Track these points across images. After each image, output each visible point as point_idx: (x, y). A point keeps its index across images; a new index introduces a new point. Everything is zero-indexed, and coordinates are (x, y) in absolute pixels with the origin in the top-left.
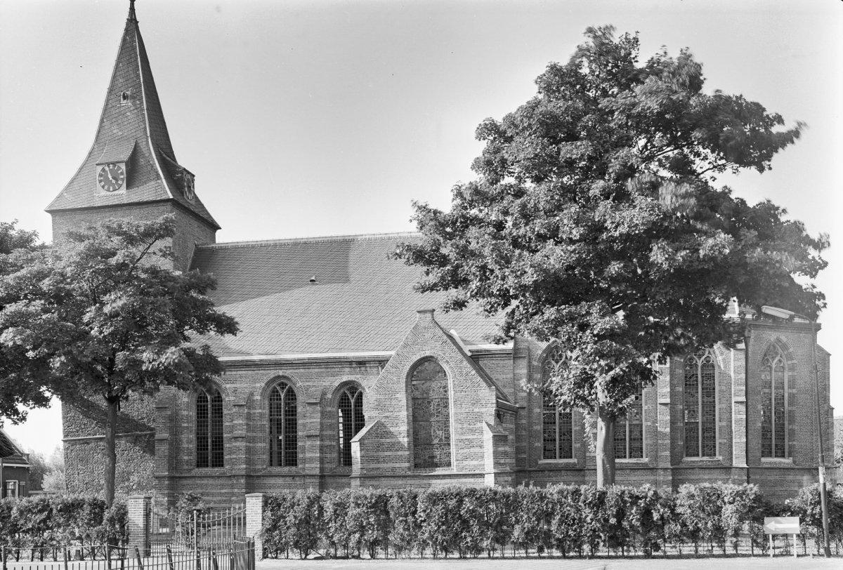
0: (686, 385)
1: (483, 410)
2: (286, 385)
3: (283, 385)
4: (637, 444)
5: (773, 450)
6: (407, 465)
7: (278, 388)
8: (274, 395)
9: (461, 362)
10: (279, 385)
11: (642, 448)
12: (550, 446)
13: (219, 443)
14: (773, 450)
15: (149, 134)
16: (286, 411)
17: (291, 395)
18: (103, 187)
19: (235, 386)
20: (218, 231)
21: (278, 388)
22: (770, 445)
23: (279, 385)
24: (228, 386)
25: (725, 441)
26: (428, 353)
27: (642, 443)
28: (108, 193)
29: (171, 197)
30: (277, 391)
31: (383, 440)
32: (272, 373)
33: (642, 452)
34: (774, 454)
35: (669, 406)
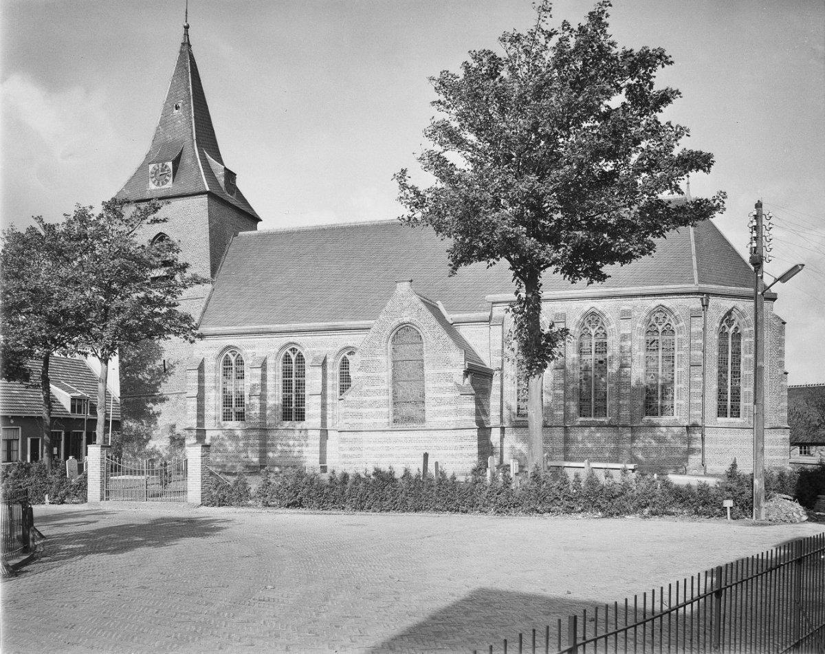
0: (647, 349)
1: (452, 371)
2: (297, 350)
3: (293, 350)
4: (602, 404)
5: (729, 412)
6: (387, 420)
7: (290, 353)
8: (287, 359)
9: (434, 327)
10: (291, 350)
11: (606, 408)
12: (600, 404)
13: (301, 400)
14: (729, 412)
15: (195, 138)
16: (296, 373)
17: (300, 359)
18: (154, 182)
19: (254, 351)
20: (259, 223)
21: (290, 353)
22: (725, 406)
23: (291, 350)
24: (248, 351)
25: (112, 478)
26: (406, 320)
27: (606, 403)
28: (158, 188)
29: (208, 189)
30: (289, 356)
31: (365, 398)
32: (285, 339)
33: (606, 412)
34: (729, 415)
35: (767, 425)
